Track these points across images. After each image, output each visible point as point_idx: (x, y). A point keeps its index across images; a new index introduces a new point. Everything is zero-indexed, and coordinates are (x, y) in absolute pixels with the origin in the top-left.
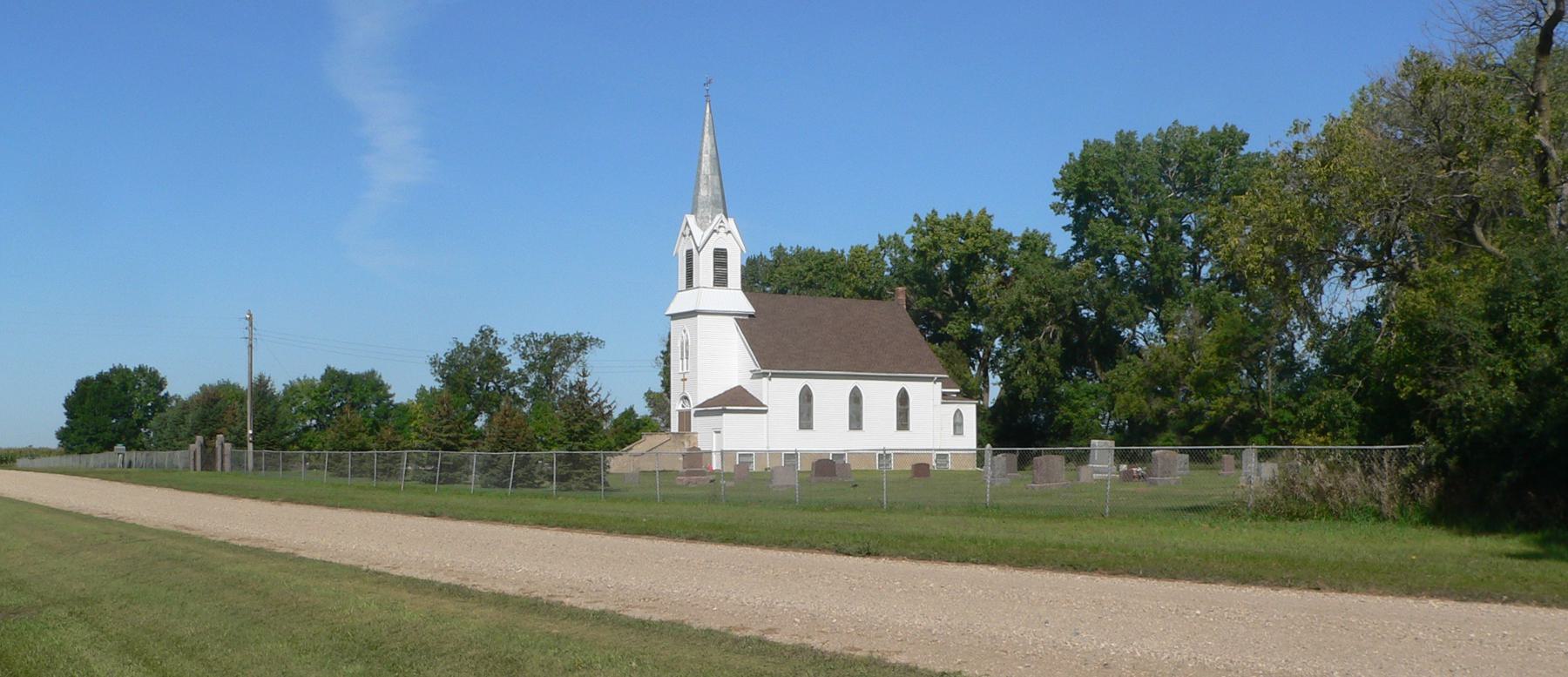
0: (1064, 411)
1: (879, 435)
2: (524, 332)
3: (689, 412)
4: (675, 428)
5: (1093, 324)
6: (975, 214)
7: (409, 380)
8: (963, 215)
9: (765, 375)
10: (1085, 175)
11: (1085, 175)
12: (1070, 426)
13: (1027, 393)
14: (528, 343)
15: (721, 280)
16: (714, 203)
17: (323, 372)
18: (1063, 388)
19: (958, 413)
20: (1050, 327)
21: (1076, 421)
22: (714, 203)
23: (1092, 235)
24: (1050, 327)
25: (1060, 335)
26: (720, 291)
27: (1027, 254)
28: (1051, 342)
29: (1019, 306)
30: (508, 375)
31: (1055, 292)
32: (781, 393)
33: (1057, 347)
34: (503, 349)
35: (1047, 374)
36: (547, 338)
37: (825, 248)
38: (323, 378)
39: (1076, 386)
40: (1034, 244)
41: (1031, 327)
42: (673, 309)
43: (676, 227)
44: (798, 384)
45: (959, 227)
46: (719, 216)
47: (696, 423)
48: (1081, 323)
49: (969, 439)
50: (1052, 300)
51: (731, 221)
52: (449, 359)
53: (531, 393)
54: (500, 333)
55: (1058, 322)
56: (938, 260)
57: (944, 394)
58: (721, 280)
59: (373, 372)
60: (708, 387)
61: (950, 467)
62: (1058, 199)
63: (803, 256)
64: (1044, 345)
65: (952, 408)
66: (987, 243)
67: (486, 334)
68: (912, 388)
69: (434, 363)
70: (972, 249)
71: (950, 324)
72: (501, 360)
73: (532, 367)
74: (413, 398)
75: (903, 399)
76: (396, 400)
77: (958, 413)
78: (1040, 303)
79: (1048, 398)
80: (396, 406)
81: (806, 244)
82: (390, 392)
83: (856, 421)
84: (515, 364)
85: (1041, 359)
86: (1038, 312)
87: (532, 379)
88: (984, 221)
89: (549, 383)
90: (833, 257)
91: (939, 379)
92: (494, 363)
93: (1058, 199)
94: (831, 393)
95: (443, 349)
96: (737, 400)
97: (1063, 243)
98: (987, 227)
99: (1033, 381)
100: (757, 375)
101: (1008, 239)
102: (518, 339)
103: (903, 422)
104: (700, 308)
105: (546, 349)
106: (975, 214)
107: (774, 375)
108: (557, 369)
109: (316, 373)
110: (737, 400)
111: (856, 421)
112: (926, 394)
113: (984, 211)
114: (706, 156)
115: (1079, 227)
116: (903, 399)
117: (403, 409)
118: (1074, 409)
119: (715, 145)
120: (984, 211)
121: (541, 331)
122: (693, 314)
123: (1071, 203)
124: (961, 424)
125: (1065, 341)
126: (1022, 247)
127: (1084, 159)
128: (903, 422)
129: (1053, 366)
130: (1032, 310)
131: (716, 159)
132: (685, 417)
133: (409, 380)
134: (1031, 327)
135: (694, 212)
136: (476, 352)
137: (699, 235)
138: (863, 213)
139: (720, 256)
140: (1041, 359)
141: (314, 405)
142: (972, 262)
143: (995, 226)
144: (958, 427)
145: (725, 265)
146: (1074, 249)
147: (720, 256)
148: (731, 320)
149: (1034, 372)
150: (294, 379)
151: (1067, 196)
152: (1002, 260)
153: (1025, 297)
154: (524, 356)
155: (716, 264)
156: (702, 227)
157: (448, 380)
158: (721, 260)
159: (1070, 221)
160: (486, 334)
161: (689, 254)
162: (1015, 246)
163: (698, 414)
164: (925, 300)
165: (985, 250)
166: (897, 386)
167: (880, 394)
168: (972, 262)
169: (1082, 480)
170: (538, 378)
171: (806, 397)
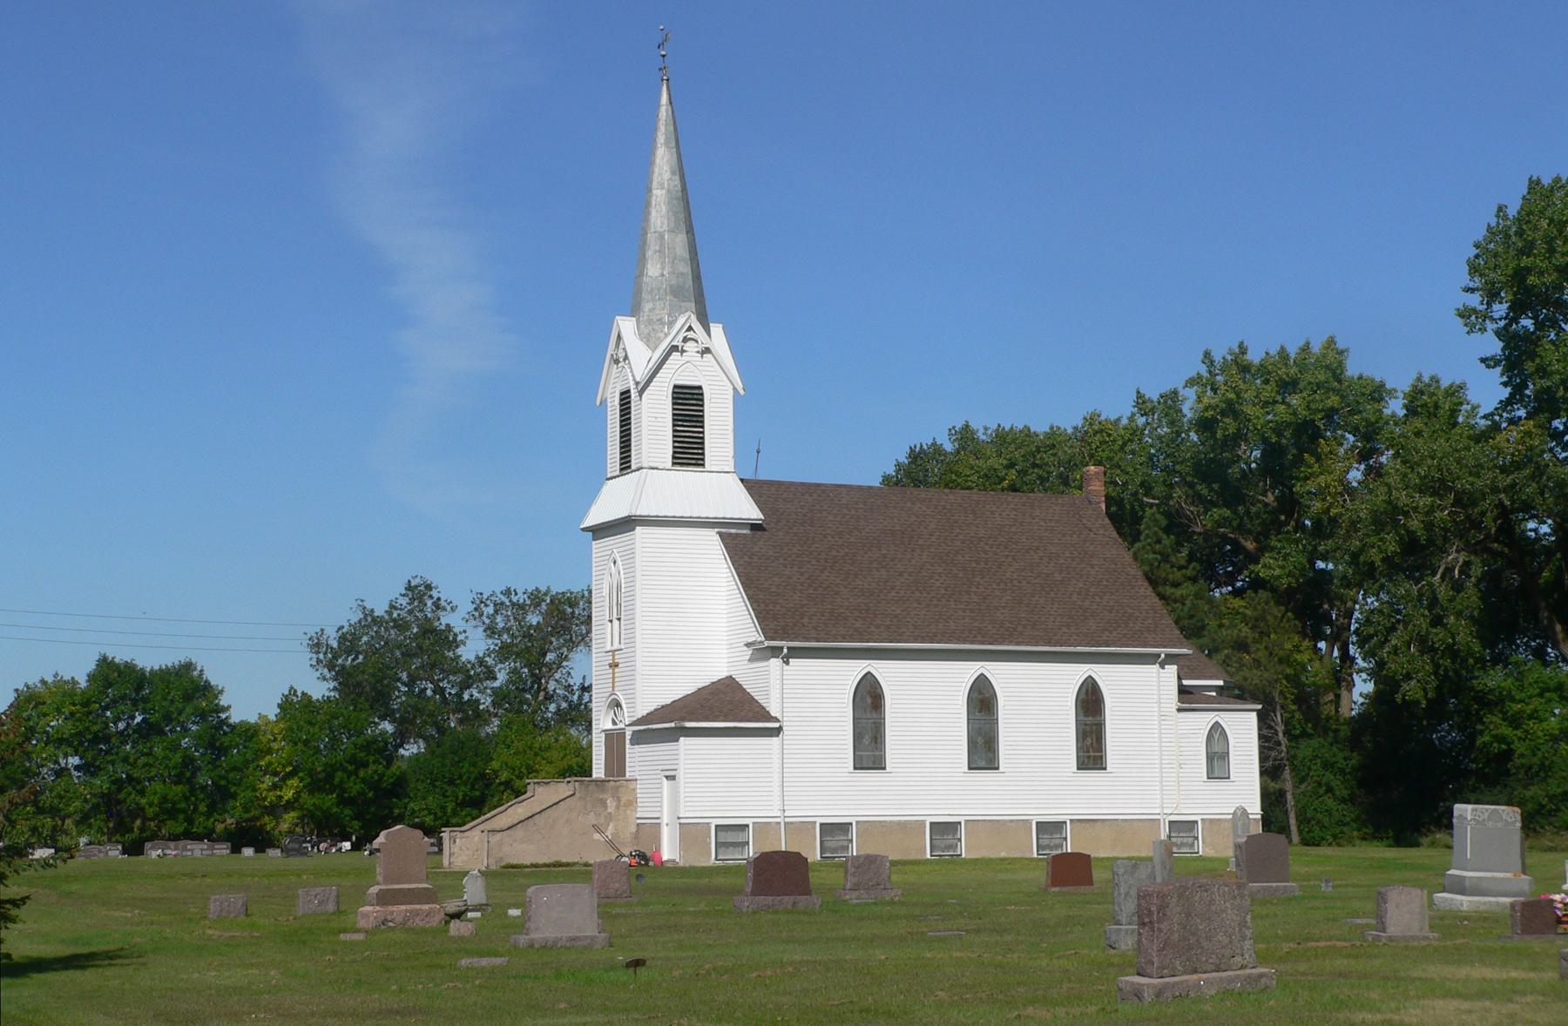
0: (1495, 726)
1: (1036, 784)
2: (492, 586)
3: (622, 735)
4: (598, 771)
5: (1549, 552)
6: (1316, 348)
7: (259, 678)
8: (1293, 352)
9: (775, 652)
10: (1527, 250)
11: (1527, 250)
12: (1507, 755)
13: (1411, 690)
14: (499, 607)
15: (689, 451)
16: (676, 292)
17: (91, 666)
18: (1494, 679)
19: (1217, 735)
20: (1455, 556)
21: (1520, 748)
22: (676, 292)
23: (1542, 372)
24: (1455, 556)
25: (1477, 570)
26: (688, 476)
27: (1418, 423)
28: (1458, 587)
29: (1388, 517)
30: (457, 668)
31: (1464, 483)
32: (812, 692)
33: (1471, 597)
34: (453, 620)
35: (1452, 652)
36: (536, 598)
37: (1040, 427)
38: (91, 678)
39: (1520, 677)
40: (1434, 405)
41: (1415, 556)
42: (595, 517)
43: (597, 348)
44: (853, 670)
45: (1284, 377)
46: (688, 318)
47: (636, 757)
48: (1524, 549)
49: (1243, 792)
50: (1458, 502)
51: (717, 330)
52: (342, 639)
53: (500, 697)
54: (443, 592)
55: (1470, 548)
56: (1238, 437)
57: (1184, 692)
58: (689, 451)
59: (189, 666)
60: (658, 680)
61: (1201, 848)
62: (1475, 300)
63: (1002, 438)
64: (1443, 592)
65: (1201, 722)
66: (1334, 400)
67: (419, 592)
68: (1109, 677)
69: (316, 645)
70: (1303, 413)
71: (1267, 559)
72: (447, 640)
73: (504, 652)
74: (272, 712)
75: (1090, 701)
76: (235, 717)
77: (1217, 735)
78: (1431, 510)
79: (1457, 694)
80: (233, 727)
81: (1014, 418)
82: (224, 701)
83: (983, 751)
84: (474, 646)
85: (1437, 621)
86: (1429, 526)
87: (502, 677)
88: (1331, 364)
89: (537, 679)
90: (1054, 440)
91: (1170, 659)
92: (436, 641)
93: (1475, 300)
94: (925, 694)
95: (336, 617)
96: (724, 709)
97: (1487, 392)
98: (1336, 372)
99: (1424, 665)
100: (761, 653)
101: (1378, 393)
102: (479, 603)
103: (1091, 753)
104: (642, 511)
105: (534, 619)
106: (1316, 348)
107: (795, 653)
108: (550, 657)
109: (79, 669)
110: (724, 709)
111: (983, 751)
112: (1141, 692)
113: (1331, 342)
114: (659, 196)
115: (1517, 358)
116: (1090, 701)
117: (248, 732)
118: (1515, 721)
119: (680, 170)
120: (1331, 342)
121: (523, 585)
122: (626, 524)
123: (1500, 309)
124: (1225, 756)
125: (1491, 581)
126: (1412, 411)
127: (1526, 216)
128: (1091, 753)
129: (1464, 635)
130: (1415, 524)
131: (684, 202)
132: (615, 741)
133: (259, 678)
134: (1415, 556)
135: (634, 311)
136: (400, 625)
137: (640, 357)
138: (1101, 360)
139: (688, 403)
140: (1437, 621)
141: (69, 729)
142: (1307, 434)
143: (1353, 369)
144: (1217, 761)
145: (699, 420)
146: (1507, 404)
147: (688, 403)
148: (711, 538)
149: (1426, 646)
150: (33, 680)
151: (1492, 295)
152: (1370, 437)
153: (1403, 498)
154: (491, 631)
155: (677, 419)
156: (649, 340)
157: (346, 680)
158: (690, 410)
159: (1495, 347)
160: (419, 592)
161: (625, 396)
162: (1396, 407)
163: (639, 738)
164: (1219, 513)
165: (1330, 414)
166: (1076, 674)
167: (1036, 694)
168: (1307, 434)
169: (1392, 929)
170: (514, 671)
171: (869, 698)
